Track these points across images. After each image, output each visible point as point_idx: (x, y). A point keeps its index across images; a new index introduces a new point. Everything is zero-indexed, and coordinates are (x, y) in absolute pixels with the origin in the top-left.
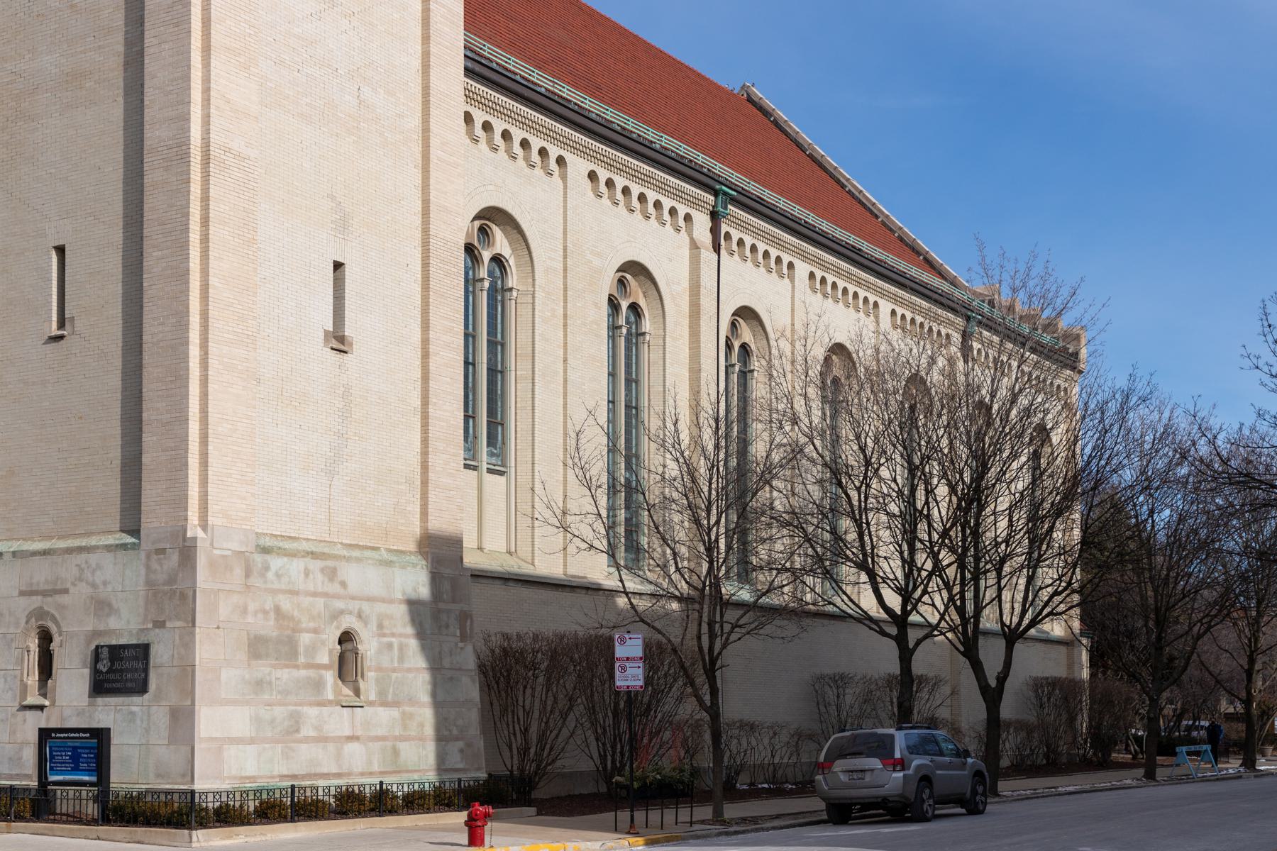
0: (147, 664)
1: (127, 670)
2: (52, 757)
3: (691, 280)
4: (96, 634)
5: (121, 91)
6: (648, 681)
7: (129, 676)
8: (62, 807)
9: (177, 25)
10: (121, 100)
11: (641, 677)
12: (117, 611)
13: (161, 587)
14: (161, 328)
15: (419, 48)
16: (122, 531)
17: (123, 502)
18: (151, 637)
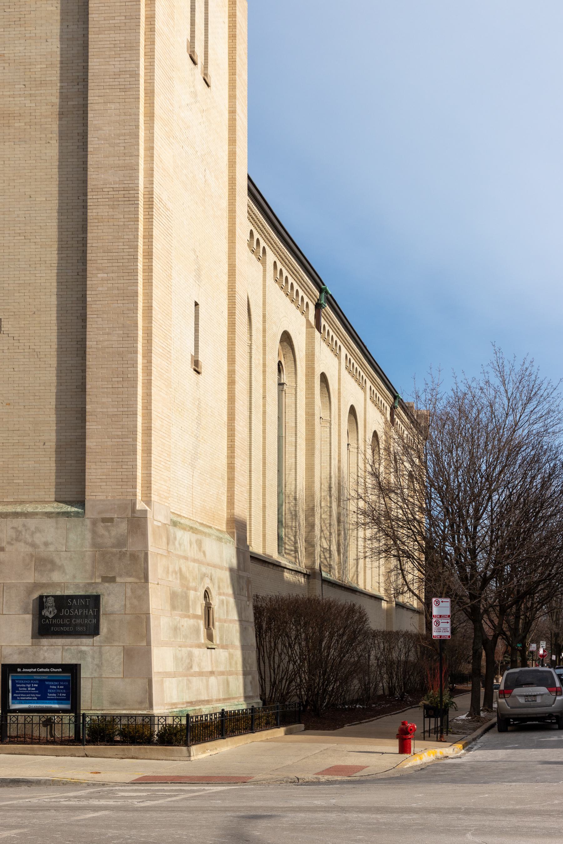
0: (98, 611)
1: (76, 617)
2: (15, 688)
3: (307, 349)
4: (36, 586)
5: (56, 136)
6: (453, 631)
7: (78, 621)
8: (12, 731)
9: (125, 90)
10: (55, 144)
11: (449, 629)
12: (61, 568)
13: (110, 549)
14: (106, 337)
15: (226, 147)
16: (56, 501)
17: (57, 477)
18: (103, 589)
